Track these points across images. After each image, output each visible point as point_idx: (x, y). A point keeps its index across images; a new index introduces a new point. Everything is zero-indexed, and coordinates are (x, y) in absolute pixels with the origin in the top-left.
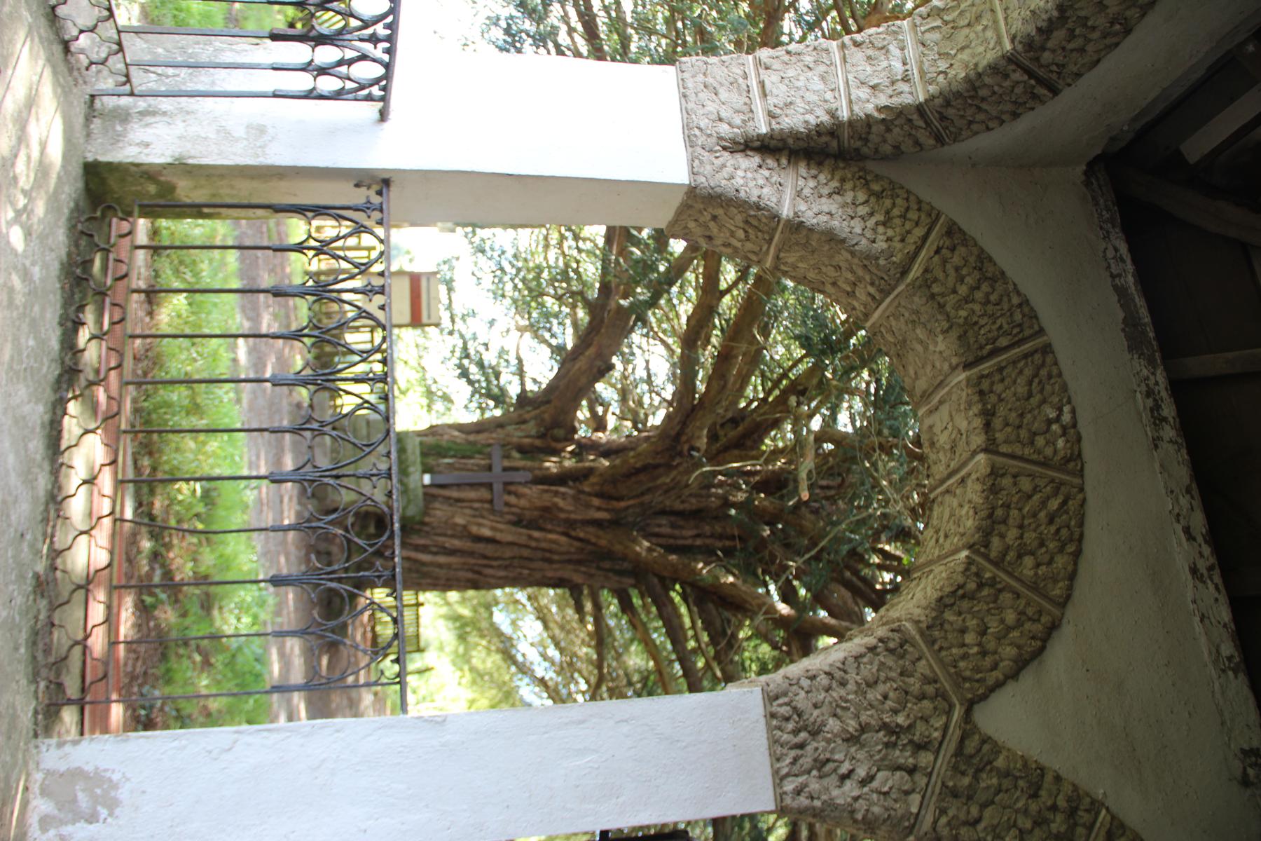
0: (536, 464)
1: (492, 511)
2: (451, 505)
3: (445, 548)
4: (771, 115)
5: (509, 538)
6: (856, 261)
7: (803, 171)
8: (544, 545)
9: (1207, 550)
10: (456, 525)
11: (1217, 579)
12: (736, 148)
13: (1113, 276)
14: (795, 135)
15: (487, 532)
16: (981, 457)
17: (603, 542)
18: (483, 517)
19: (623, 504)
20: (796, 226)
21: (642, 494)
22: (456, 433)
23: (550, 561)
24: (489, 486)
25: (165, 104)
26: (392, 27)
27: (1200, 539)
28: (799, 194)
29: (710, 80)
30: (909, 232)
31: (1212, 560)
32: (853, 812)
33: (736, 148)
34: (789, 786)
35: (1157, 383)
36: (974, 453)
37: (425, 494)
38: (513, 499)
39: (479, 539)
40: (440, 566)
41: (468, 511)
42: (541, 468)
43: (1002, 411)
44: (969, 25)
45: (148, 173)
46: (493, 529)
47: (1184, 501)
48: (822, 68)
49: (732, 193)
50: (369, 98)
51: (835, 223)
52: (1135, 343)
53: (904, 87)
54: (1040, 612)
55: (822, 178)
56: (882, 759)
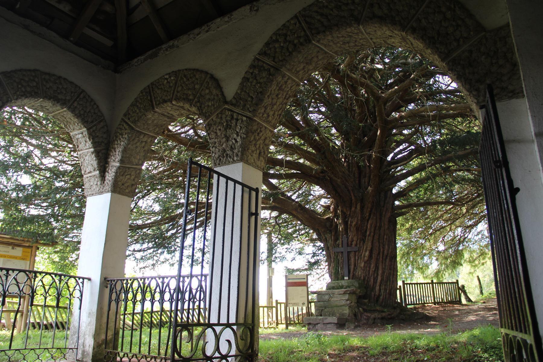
0: (341, 234)
1: (359, 250)
2: (357, 268)
3: (375, 270)
4: (94, 170)
5: (370, 244)
6: (131, 143)
7: (109, 160)
8: (372, 230)
9: (203, 28)
10: (364, 266)
11: (209, 24)
12: (103, 179)
13: (141, 63)
14: (99, 164)
15: (367, 254)
16: (174, 103)
17: (370, 205)
18: (361, 255)
19: (353, 198)
20: (122, 161)
21: (348, 190)
22: (331, 267)
23: (380, 227)
24: (349, 253)
25: (81, 341)
26: (79, 278)
27: (200, 30)
28: (114, 161)
29: (89, 188)
30: (125, 128)
31: (206, 25)
32: (244, 138)
33: (103, 179)
34: (235, 158)
35: (165, 47)
36: (173, 104)
37: (352, 279)
38: (354, 243)
39: (370, 256)
40: (383, 273)
41: (359, 261)
42: (342, 232)
43: (164, 97)
44: (65, 118)
45: (97, 346)
46: (366, 251)
47: (191, 36)
48: (84, 156)
49: (113, 180)
50: (83, 283)
51: (121, 150)
52: (155, 55)
53: (84, 133)
54: (207, 82)
55: (112, 154)
56: (233, 130)
